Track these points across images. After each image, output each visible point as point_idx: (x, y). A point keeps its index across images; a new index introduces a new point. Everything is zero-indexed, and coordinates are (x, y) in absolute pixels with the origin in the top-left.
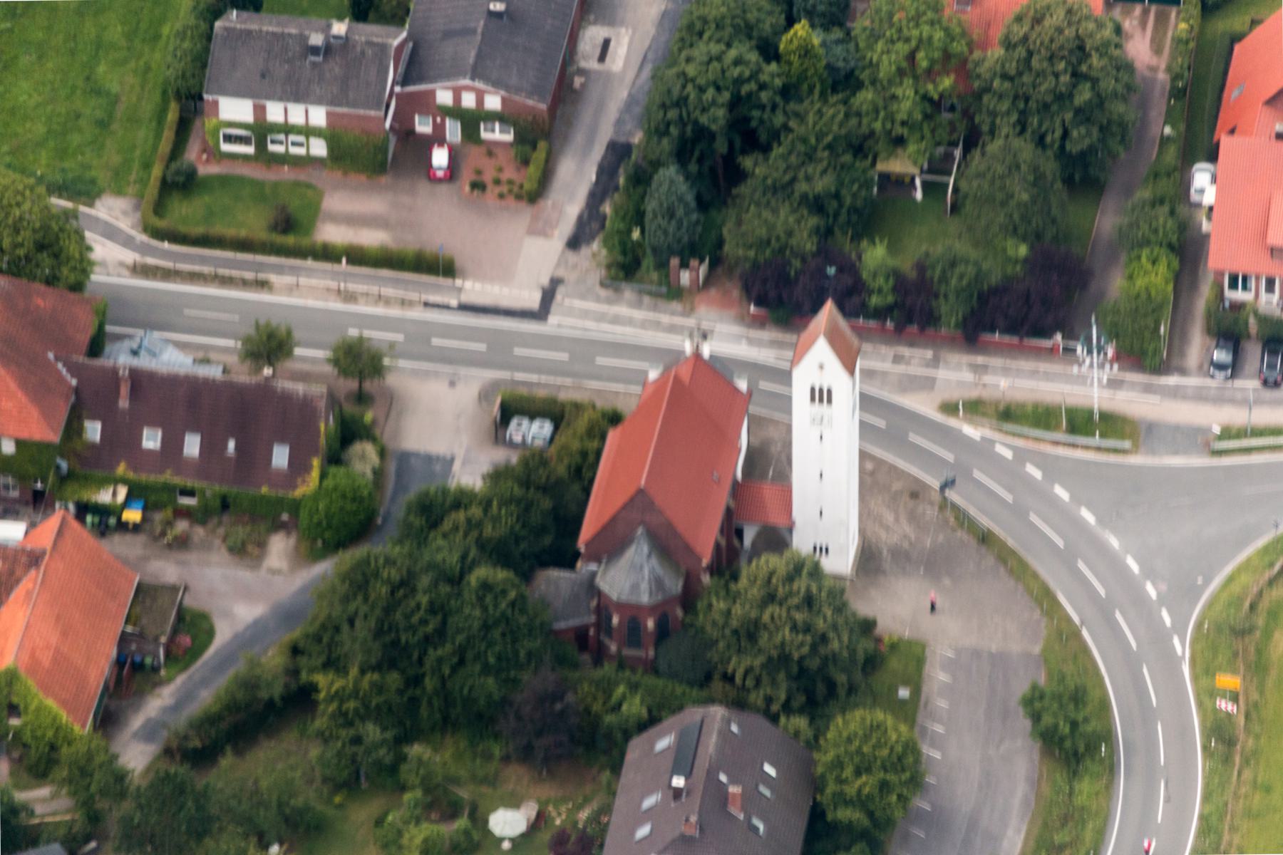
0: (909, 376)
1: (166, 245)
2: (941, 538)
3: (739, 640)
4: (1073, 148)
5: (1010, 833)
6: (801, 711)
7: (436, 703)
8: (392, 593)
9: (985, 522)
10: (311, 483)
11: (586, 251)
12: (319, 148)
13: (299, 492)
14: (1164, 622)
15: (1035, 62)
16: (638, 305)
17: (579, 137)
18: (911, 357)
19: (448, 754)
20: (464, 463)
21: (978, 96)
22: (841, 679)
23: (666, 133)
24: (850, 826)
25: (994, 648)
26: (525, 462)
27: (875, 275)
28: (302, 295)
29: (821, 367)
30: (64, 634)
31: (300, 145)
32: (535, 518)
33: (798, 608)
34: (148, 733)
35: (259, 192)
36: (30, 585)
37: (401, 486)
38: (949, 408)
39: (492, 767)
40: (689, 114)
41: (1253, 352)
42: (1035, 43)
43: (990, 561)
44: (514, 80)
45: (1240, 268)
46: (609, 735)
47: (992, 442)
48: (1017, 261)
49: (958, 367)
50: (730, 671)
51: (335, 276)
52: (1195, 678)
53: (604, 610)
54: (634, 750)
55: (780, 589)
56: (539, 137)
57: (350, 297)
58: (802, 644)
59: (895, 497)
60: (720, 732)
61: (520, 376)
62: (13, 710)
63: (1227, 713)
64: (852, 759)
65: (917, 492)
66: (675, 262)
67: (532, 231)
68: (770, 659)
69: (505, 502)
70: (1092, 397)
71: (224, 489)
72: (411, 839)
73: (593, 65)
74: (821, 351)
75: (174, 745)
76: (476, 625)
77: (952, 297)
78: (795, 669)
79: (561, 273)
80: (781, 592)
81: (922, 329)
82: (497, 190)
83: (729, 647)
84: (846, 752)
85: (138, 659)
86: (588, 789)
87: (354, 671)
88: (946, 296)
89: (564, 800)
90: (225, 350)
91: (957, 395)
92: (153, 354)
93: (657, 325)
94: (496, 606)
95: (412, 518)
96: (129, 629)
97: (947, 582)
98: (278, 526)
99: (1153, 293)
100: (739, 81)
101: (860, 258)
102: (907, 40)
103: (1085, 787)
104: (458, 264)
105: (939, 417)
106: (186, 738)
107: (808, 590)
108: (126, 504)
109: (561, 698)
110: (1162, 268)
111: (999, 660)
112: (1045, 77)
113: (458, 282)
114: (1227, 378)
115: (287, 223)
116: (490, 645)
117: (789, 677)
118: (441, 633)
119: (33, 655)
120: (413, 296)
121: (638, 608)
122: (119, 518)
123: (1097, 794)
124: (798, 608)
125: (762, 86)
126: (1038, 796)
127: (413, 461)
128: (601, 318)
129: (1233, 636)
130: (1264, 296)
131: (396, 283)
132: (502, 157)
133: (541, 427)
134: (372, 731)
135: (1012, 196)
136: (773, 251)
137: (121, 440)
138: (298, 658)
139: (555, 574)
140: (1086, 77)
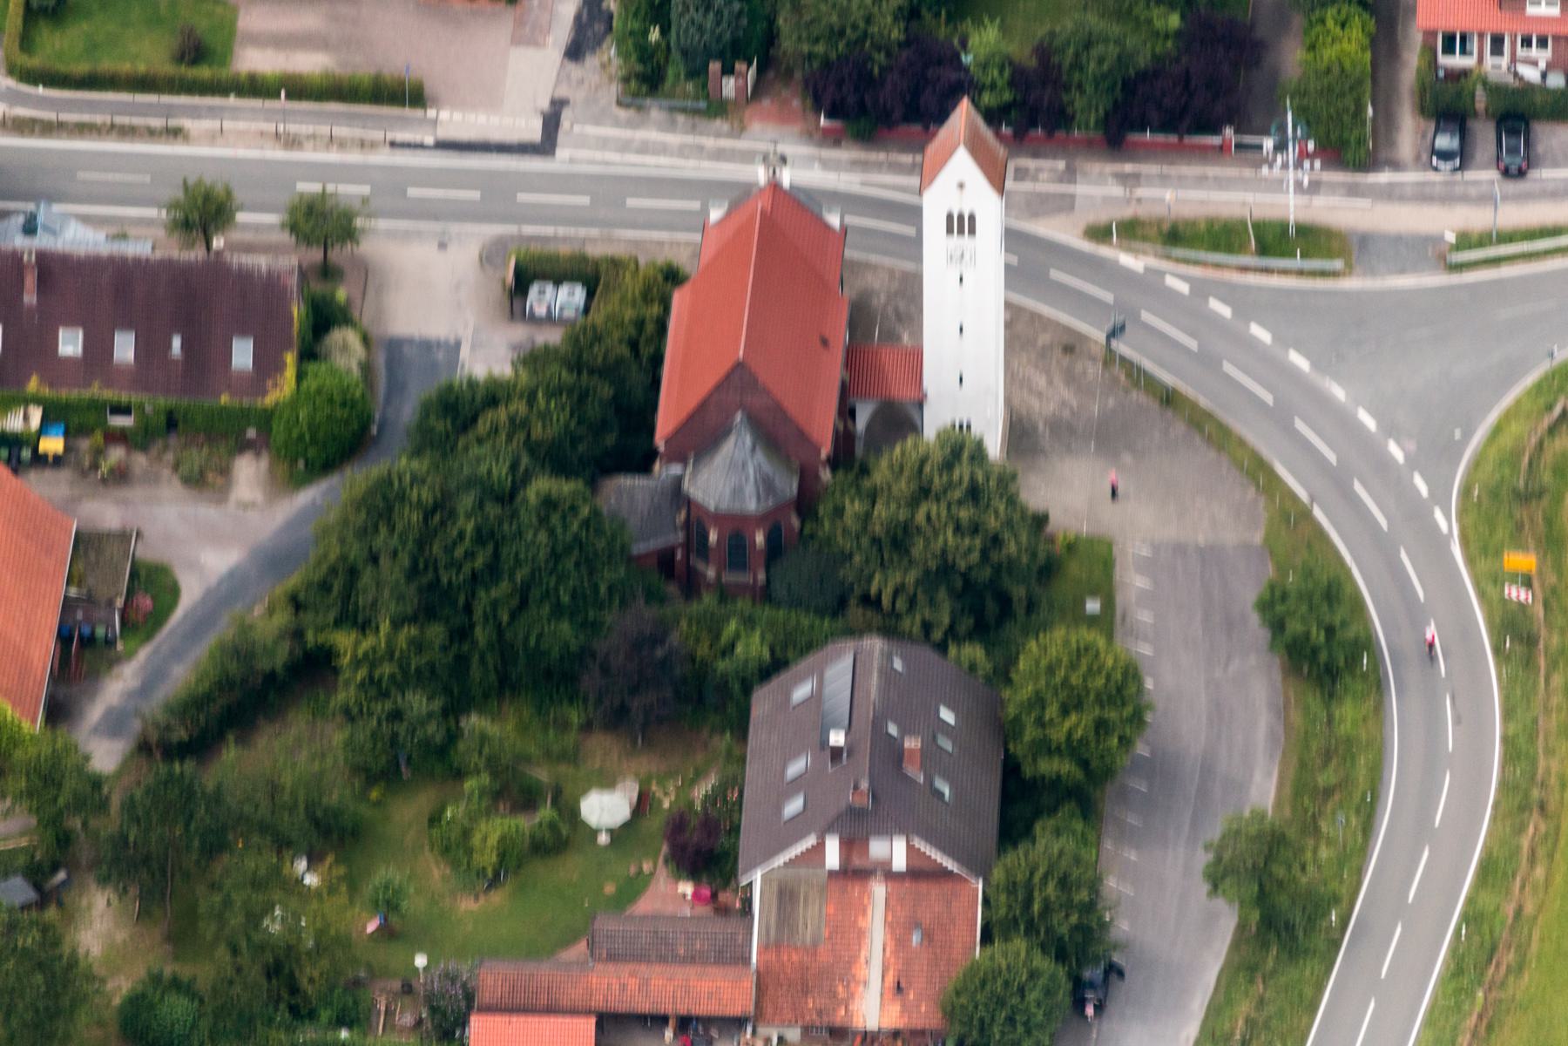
0: (1039, 195)
1: (41, 90)
2: (1111, 402)
3: (880, 550)
5: (1258, 777)
6: (971, 636)
7: (490, 660)
8: (426, 519)
9: (1167, 378)
11: (592, 61)
13: (270, 400)
14: (1418, 491)
16: (671, 127)
18: (1038, 170)
19: (510, 727)
20: (473, 347)
22: (1019, 592)
24: (1056, 781)
25: (1201, 539)
26: (574, 340)
27: (985, 66)
28: (225, 141)
29: (961, 186)
32: (593, 411)
33: (960, 503)
34: (113, 725)
37: (396, 388)
38: (1099, 233)
39: (571, 738)
41: (1485, 134)
43: (1179, 428)
45: (1456, 24)
46: (723, 687)
47: (1161, 274)
48: (1167, 36)
49: (1101, 180)
50: (874, 590)
51: (268, 116)
52: (1470, 561)
53: (696, 523)
54: (762, 702)
55: (936, 480)
57: (292, 142)
58: (970, 550)
59: (1044, 353)
60: (880, 671)
61: (529, 230)
63: (1520, 603)
64: (1056, 694)
65: (1071, 346)
66: (715, 67)
67: (517, 41)
68: (927, 572)
69: (554, 393)
70: (1287, 206)
72: (485, 839)
74: (962, 165)
75: (154, 737)
76: (542, 555)
77: (1089, 89)
78: (959, 584)
79: (563, 92)
81: (1050, 133)
83: (867, 561)
84: (1048, 684)
85: (86, 631)
86: (700, 758)
87: (385, 627)
88: (1080, 86)
89: (670, 774)
90: (149, 222)
91: (1102, 216)
92: (53, 233)
93: (700, 151)
94: (565, 527)
95: (432, 421)
96: (73, 592)
97: (1127, 458)
98: (243, 446)
99: (1347, 65)
103: (1348, 712)
104: (428, 91)
105: (1087, 246)
106: (168, 728)
107: (973, 480)
108: (42, 431)
109: (662, 642)
111: (1210, 556)
113: (431, 113)
114: (1455, 170)
115: (195, 51)
117: (952, 592)
118: (494, 570)
120: (378, 135)
122: (35, 449)
123: (1365, 719)
124: (960, 503)
126: (1288, 726)
127: (406, 349)
128: (624, 147)
130: (1489, 60)
131: (351, 119)
133: (571, 294)
134: (418, 703)
136: (848, 45)
138: (301, 614)
139: (626, 482)
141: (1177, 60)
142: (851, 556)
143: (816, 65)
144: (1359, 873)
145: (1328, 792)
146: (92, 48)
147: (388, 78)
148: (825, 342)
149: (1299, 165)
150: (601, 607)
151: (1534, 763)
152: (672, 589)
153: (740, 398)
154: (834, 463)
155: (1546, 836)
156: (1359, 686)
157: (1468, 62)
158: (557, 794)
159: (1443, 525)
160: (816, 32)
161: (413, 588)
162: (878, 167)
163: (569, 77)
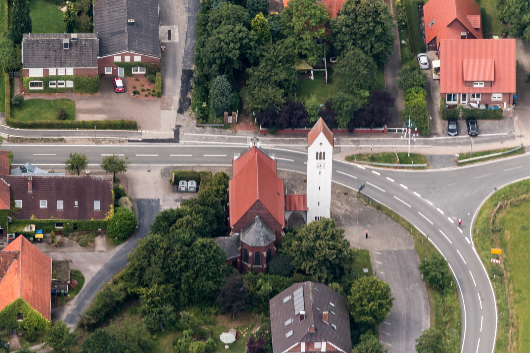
4: (375, 52)
5: (424, 319)
8: (165, 253)
10: (110, 215)
11: (186, 114)
12: (70, 84)
15: (359, 19)
16: (214, 132)
17: (170, 70)
20: (163, 202)
21: (334, 35)
22: (346, 266)
23: (214, 62)
27: (311, 109)
28: (78, 142)
30: (33, 284)
31: (63, 84)
32: (210, 218)
33: (329, 241)
34: (71, 319)
35: (49, 105)
36: (17, 266)
37: (142, 214)
38: (350, 159)
40: (223, 54)
41: (463, 124)
42: (358, 11)
43: (384, 216)
44: (145, 49)
46: (259, 300)
52: (479, 252)
53: (244, 250)
54: (273, 303)
56: (155, 70)
57: (98, 142)
58: (333, 254)
62: (20, 316)
66: (226, 113)
67: (162, 109)
73: (167, 41)
74: (322, 138)
77: (344, 115)
79: (179, 123)
80: (322, 234)
82: (144, 93)
91: (350, 154)
97: (369, 226)
98: (98, 234)
100: (242, 39)
101: (304, 103)
102: (305, 16)
103: (449, 299)
110: (422, 95)
111: (399, 253)
112: (363, 25)
113: (139, 131)
114: (456, 135)
115: (64, 115)
116: (209, 268)
118: (187, 267)
119: (26, 293)
121: (260, 248)
122: (34, 237)
125: (251, 40)
126: (431, 304)
128: (200, 139)
129: (490, 233)
130: (462, 102)
132: (143, 81)
133: (192, 183)
135: (360, 72)
137: (31, 206)
139: (222, 238)
140: (379, 23)
141: (369, 105)
142: (294, 258)
143: (259, 111)
144: (460, 346)
145: (446, 323)
146: (32, 116)
147: (126, 122)
148: (279, 194)
149: (412, 135)
150: (220, 276)
151: (508, 311)
152: (235, 270)
153: (258, 212)
154: (285, 231)
155: (515, 333)
156: (451, 291)
157: (456, 103)
158: (212, 333)
159: (469, 242)
160: (258, 101)
161: (163, 274)
162: (279, 141)
163: (180, 118)
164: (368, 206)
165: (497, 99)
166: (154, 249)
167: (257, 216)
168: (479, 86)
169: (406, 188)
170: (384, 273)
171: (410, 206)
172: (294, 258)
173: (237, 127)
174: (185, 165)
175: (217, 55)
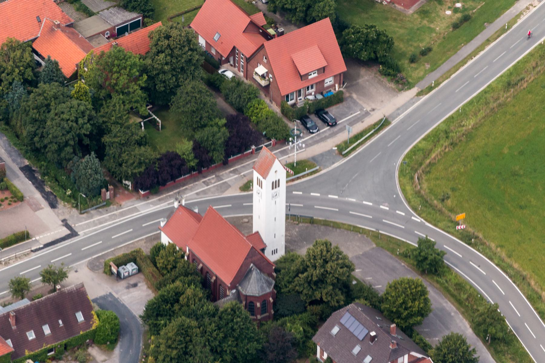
2: (297, 230)
5: (445, 304)
15: (177, 52)
16: (101, 214)
25: (361, 253)
40: (75, 133)
43: (322, 228)
52: (435, 225)
71: (64, 341)
98: (88, 346)
113: (34, 239)
114: (318, 131)
142: (301, 292)
159: (419, 221)
164: (301, 225)
165: (329, 84)
166: (186, 331)
167: (252, 265)
168: (313, 76)
169: (319, 195)
170: (371, 278)
171: (337, 210)
172: (301, 292)
173: (117, 200)
174: (103, 253)
175: (69, 136)
